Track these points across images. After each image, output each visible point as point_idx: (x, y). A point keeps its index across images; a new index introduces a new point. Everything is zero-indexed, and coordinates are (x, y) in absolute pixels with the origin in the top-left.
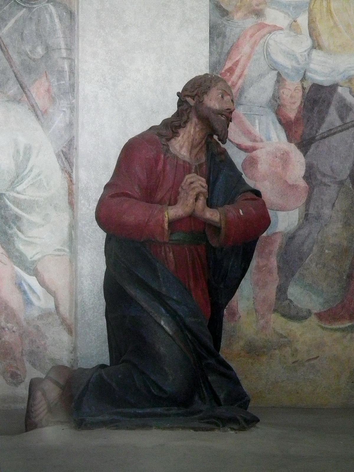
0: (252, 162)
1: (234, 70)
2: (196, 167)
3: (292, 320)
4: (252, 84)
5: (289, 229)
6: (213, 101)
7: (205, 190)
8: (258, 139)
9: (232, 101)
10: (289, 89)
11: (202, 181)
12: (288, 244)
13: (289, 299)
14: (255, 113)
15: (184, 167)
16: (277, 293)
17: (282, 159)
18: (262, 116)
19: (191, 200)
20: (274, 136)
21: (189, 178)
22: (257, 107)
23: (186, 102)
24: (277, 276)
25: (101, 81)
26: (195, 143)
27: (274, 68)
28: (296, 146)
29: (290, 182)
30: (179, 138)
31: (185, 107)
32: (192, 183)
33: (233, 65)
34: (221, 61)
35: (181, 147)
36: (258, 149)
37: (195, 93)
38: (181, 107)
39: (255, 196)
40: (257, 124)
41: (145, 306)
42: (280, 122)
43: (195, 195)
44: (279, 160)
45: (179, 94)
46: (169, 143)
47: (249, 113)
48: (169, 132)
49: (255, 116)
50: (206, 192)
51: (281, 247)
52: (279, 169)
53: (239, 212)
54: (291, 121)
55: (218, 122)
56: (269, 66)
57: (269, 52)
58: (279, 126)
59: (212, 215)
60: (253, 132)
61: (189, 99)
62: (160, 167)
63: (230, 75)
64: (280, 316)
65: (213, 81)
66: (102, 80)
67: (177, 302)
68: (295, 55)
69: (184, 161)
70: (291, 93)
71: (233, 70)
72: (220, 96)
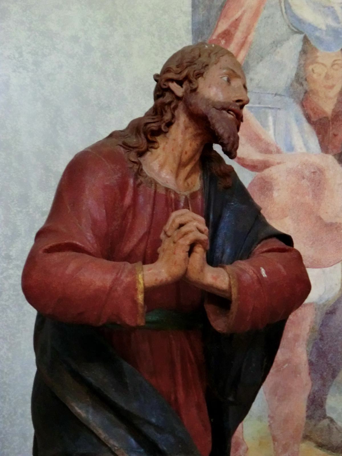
0: (266, 186)
1: (232, 34)
2: (186, 199)
3: (334, 453)
4: (261, 58)
5: (326, 297)
6: (212, 90)
7: (204, 237)
8: (272, 148)
9: (245, 87)
10: (323, 64)
11: (199, 221)
12: (324, 324)
13: (329, 418)
14: (267, 106)
15: (167, 200)
16: (308, 408)
17: (313, 181)
18: (278, 111)
19: (181, 254)
20: (298, 142)
21: (178, 216)
22: (270, 96)
23: (169, 90)
24: (308, 378)
25: (14, 58)
26: (185, 158)
27: (298, 29)
28: (335, 158)
29: (327, 218)
30: (159, 151)
31: (168, 98)
32: (181, 225)
33: (231, 26)
34: (211, 21)
35: (162, 166)
36: (273, 165)
37: (184, 74)
38: (161, 100)
39: (280, 244)
40: (271, 124)
41: (103, 435)
42: (309, 119)
43: (189, 245)
44: (308, 184)
45: (157, 78)
46: (141, 160)
47: (258, 105)
48: (142, 142)
49: (267, 110)
50: (207, 240)
51: (313, 328)
52: (308, 199)
53: (259, 271)
54: (327, 118)
55: (221, 124)
56: (289, 26)
57: (289, 4)
58: (307, 126)
59: (215, 278)
60: (263, 137)
61: (174, 86)
62: (128, 200)
63: (226, 43)
64: (315, 446)
65: (212, 55)
66: (17, 56)
67: (159, 429)
68: (332, 7)
69: (167, 190)
70: (326, 71)
71: (230, 34)
72: (225, 78)
